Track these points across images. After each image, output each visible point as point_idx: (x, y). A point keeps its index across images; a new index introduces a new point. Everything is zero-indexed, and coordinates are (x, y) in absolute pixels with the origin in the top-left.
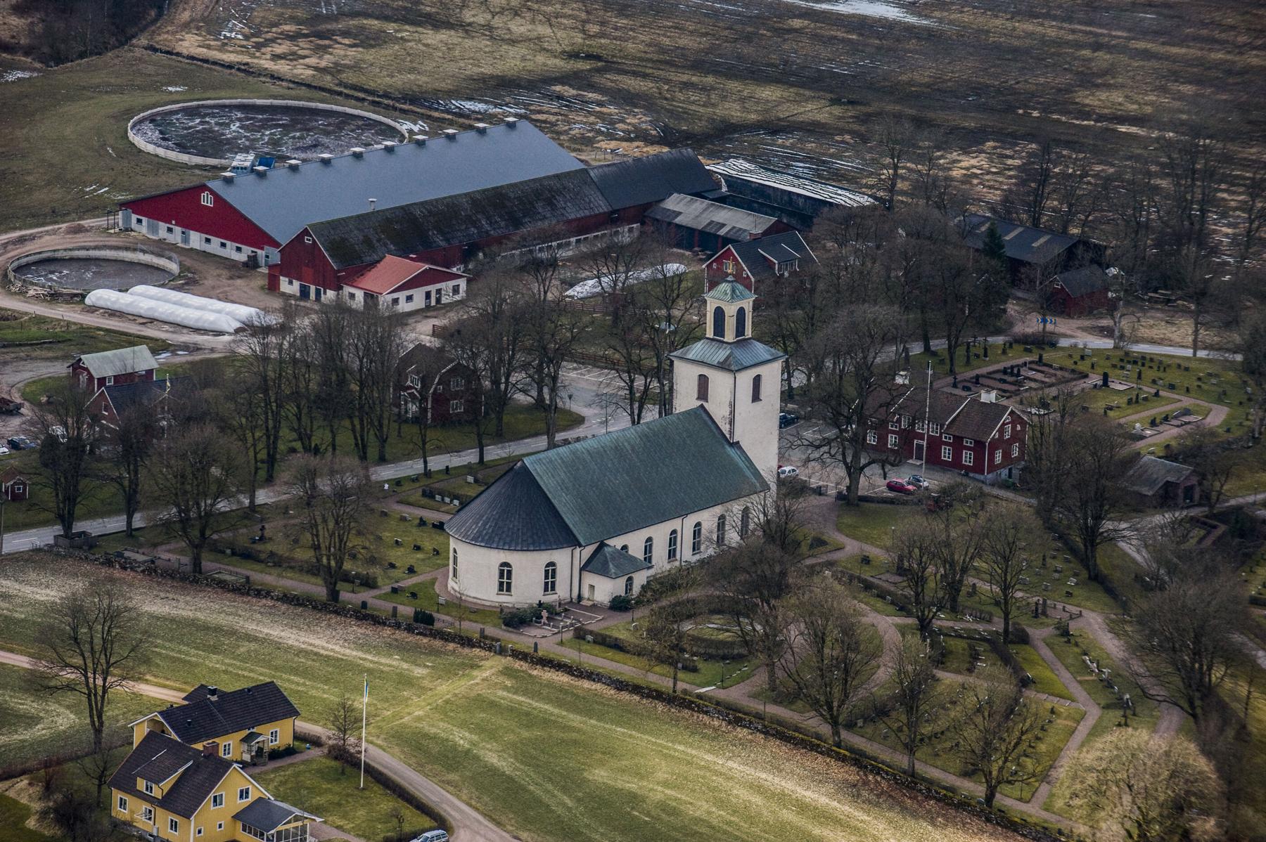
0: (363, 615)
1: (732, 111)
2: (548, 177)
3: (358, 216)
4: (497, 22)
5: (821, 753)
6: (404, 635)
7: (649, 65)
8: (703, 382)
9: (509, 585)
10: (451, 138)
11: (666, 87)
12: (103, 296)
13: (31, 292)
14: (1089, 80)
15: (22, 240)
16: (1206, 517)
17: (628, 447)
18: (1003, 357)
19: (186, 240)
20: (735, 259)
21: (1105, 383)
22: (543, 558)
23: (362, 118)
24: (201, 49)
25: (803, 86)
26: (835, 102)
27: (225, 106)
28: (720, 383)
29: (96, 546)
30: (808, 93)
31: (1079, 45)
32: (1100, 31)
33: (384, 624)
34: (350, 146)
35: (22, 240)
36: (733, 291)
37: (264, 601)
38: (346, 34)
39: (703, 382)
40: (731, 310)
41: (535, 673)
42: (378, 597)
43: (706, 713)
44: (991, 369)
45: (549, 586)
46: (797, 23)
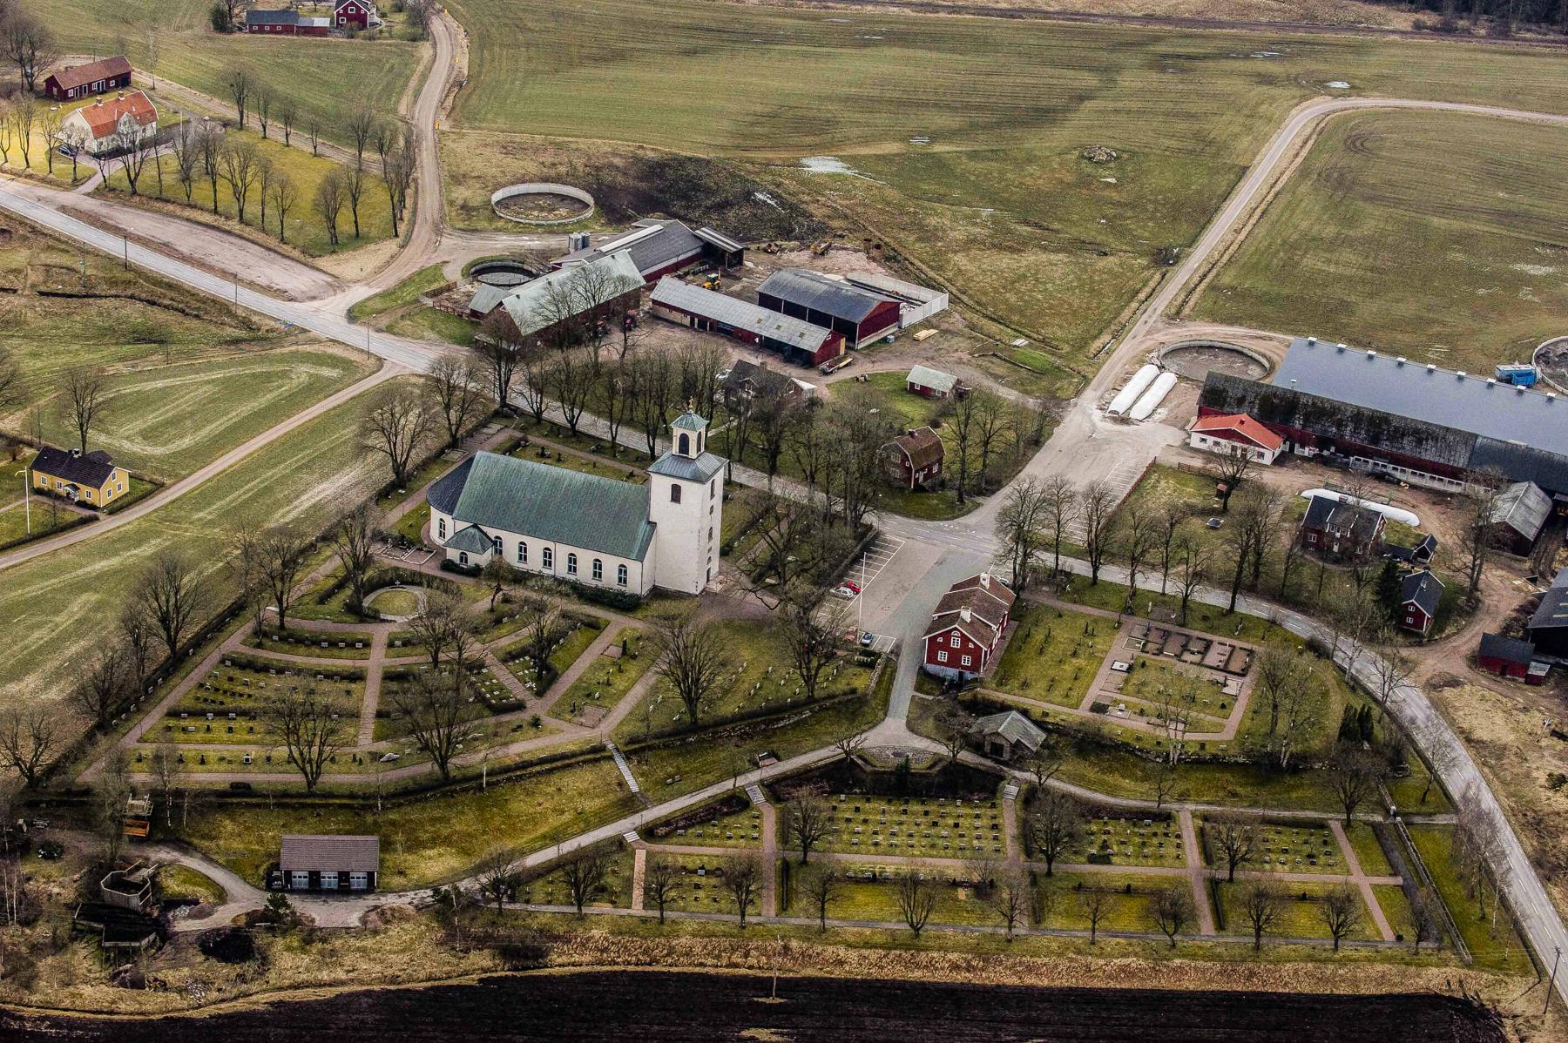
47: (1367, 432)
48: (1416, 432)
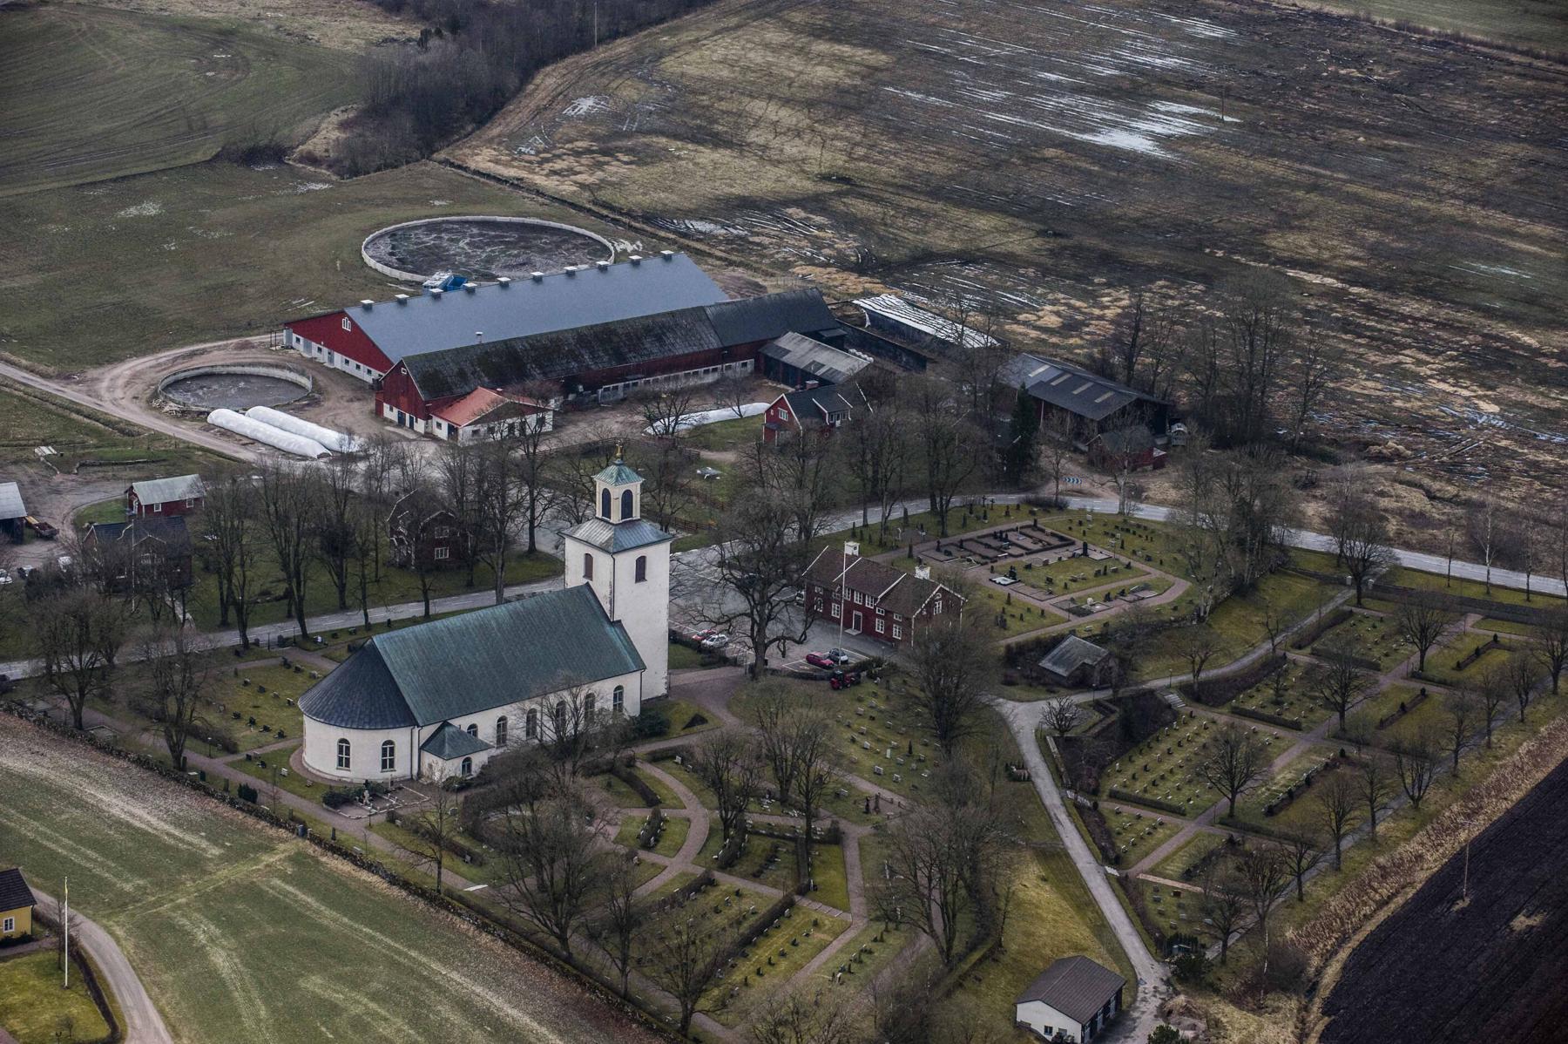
0: (202, 785)
1: (940, 239)
2: (664, 315)
3: (457, 349)
4: (775, 143)
5: (549, 966)
6: (225, 810)
7: (891, 190)
8: (589, 560)
9: (348, 760)
10: (668, 258)
11: (892, 213)
12: (223, 416)
13: (167, 409)
14: (1286, 222)
15: (193, 354)
16: (1110, 701)
17: (494, 625)
18: (1004, 520)
19: (331, 360)
20: (788, 409)
21: (1085, 554)
22: (380, 736)
23: (584, 236)
24: (490, 164)
25: (1018, 216)
26: (1040, 233)
27: (467, 222)
28: (602, 562)
29: (11, 690)
30: (1021, 223)
31: (1296, 186)
32: (1323, 172)
33: (212, 795)
34: (563, 265)
35: (193, 354)
36: (619, 474)
37: (121, 762)
38: (629, 151)
39: (589, 560)
40: (617, 493)
41: (324, 859)
42: (232, 765)
43: (460, 915)
44: (980, 533)
45: (388, 763)
46: (1050, 152)
47: (605, 351)
48: (648, 330)
